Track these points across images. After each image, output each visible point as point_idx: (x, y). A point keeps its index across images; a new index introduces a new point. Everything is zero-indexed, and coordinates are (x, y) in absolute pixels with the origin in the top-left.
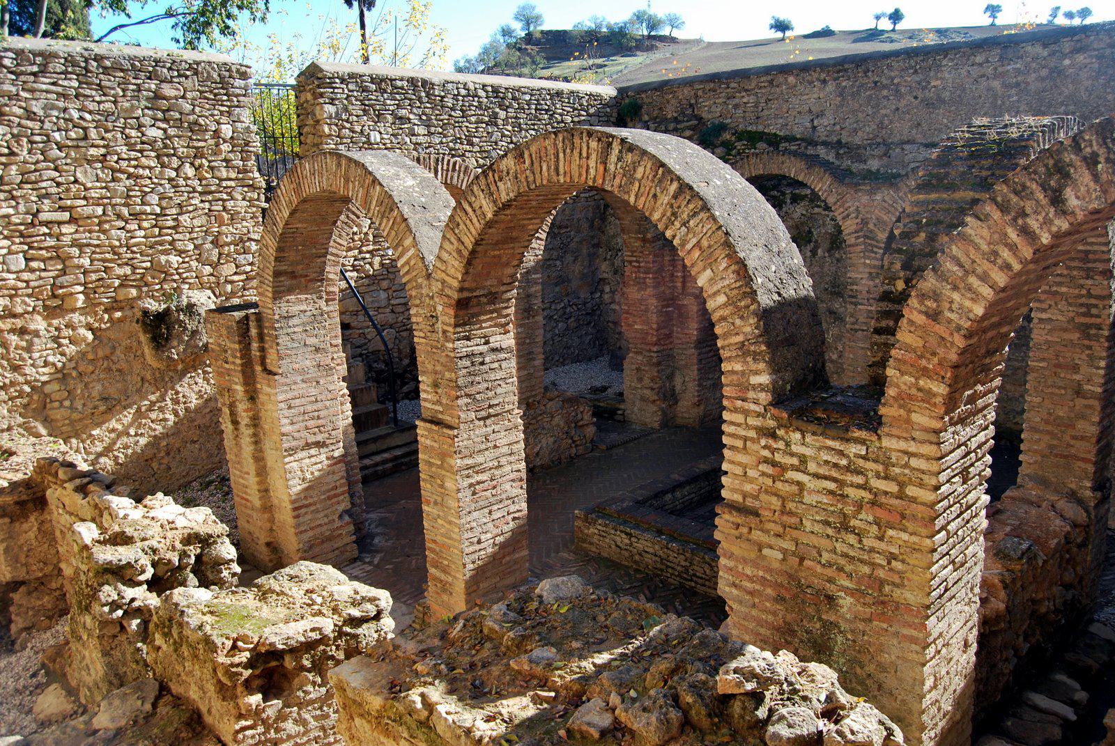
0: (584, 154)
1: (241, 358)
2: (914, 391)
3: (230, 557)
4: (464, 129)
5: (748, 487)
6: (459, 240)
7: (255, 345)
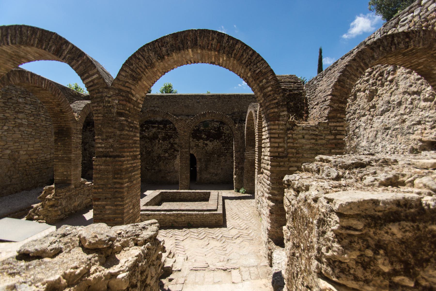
2: (338, 108)
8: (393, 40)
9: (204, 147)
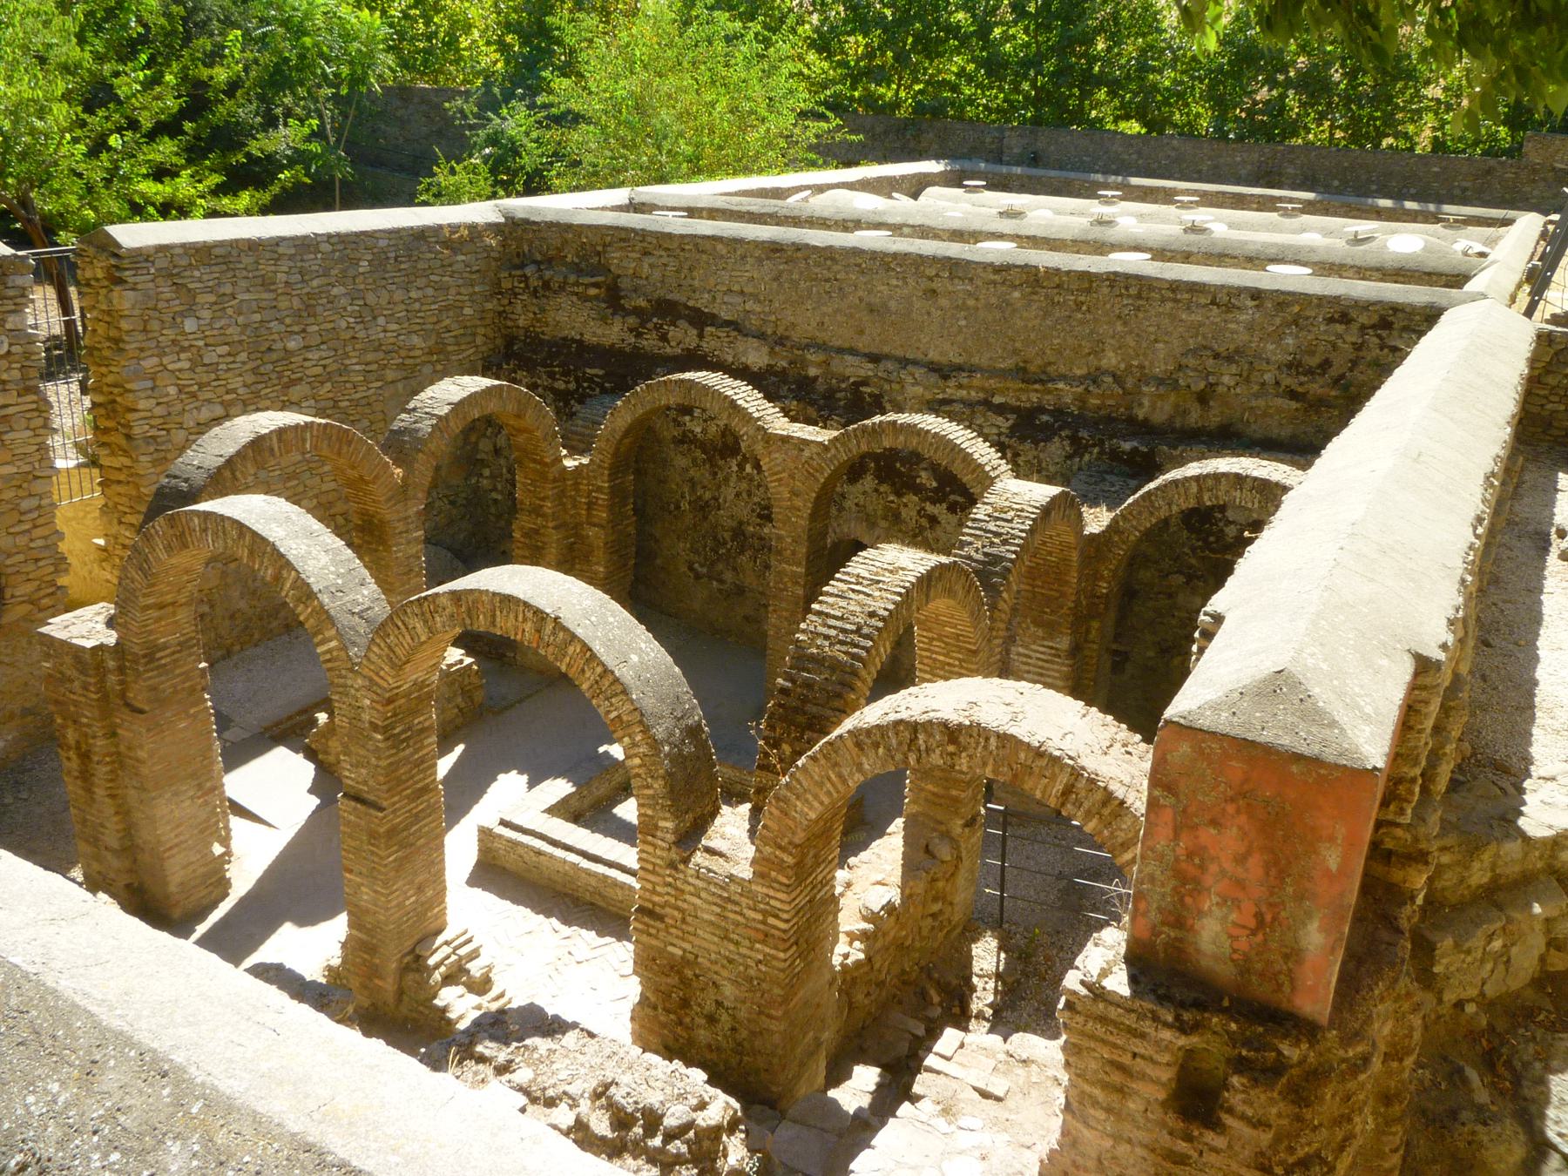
5: (656, 899)
8: (914, 740)
9: (922, 529)
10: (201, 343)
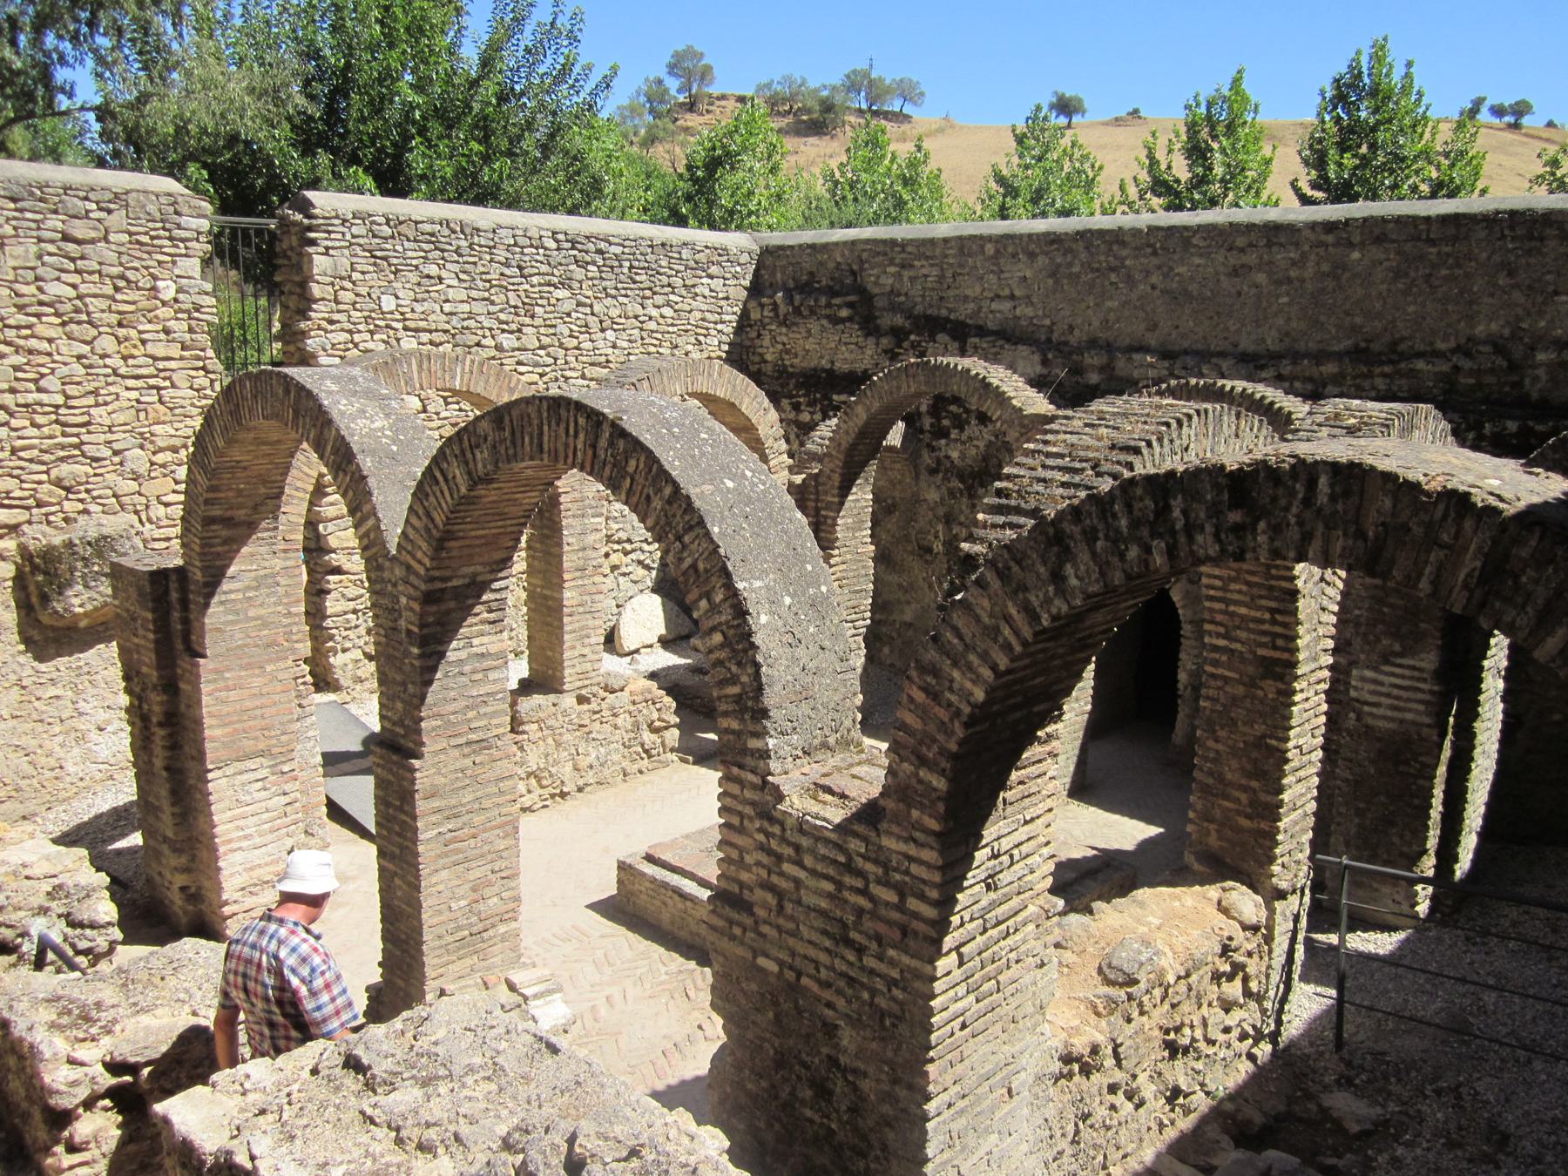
0: (572, 432)
1: (155, 632)
3: (108, 919)
4: (523, 294)
6: (428, 514)
7: (176, 615)
8: (1163, 511)
10: (399, 326)
